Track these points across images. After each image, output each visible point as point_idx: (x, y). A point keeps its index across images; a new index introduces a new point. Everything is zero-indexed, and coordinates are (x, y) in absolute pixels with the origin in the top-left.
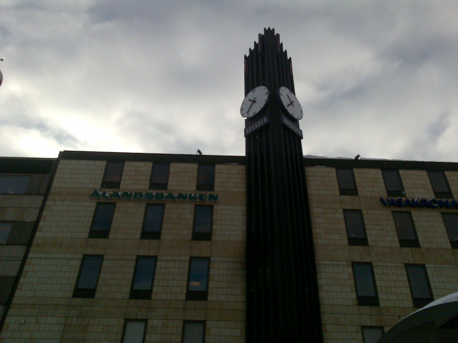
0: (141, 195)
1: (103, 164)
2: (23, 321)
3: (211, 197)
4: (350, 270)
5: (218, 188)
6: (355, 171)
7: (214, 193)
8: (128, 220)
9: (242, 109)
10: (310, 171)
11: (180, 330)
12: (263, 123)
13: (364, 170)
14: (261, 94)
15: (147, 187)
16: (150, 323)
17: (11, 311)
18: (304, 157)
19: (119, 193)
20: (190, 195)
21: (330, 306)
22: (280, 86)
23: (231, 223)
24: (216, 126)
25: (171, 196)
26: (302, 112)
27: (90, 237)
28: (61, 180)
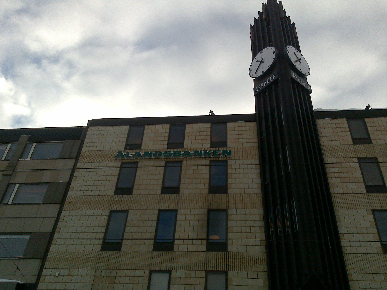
0: (161, 153)
1: (125, 129)
2: (58, 273)
3: (225, 152)
4: (371, 218)
5: (230, 145)
6: (367, 120)
7: (228, 149)
8: (149, 178)
9: (250, 71)
10: (320, 123)
11: (203, 281)
12: (272, 79)
13: (375, 119)
14: (269, 54)
15: (166, 147)
16: (173, 274)
17: (47, 265)
18: (314, 111)
19: (141, 153)
20: (205, 151)
21: (354, 254)
22: (286, 45)
23: (245, 178)
24: (228, 89)
25: (187, 153)
26: (309, 69)
27: (116, 193)
28: (90, 144)
